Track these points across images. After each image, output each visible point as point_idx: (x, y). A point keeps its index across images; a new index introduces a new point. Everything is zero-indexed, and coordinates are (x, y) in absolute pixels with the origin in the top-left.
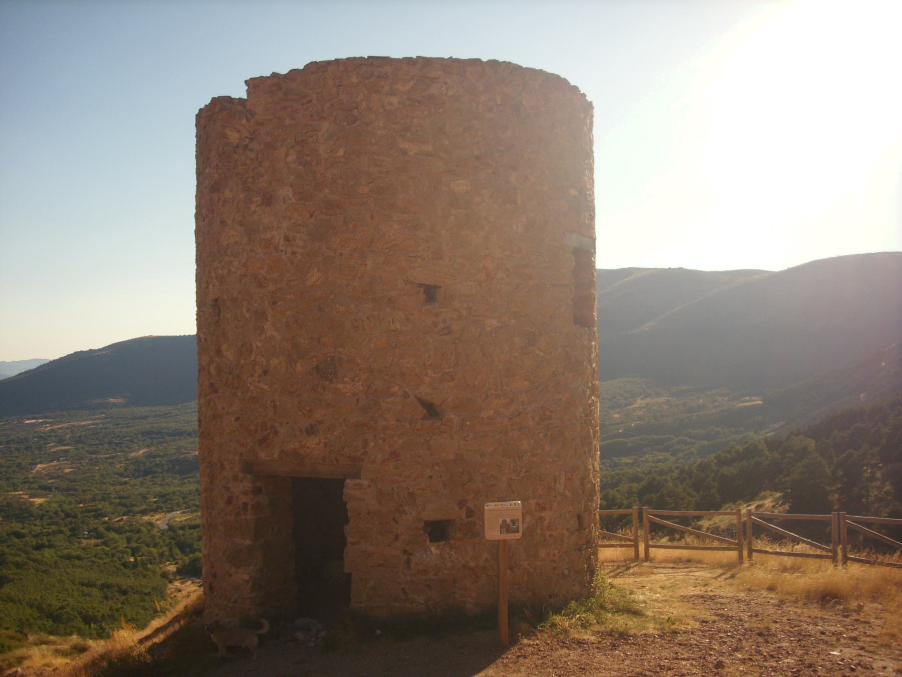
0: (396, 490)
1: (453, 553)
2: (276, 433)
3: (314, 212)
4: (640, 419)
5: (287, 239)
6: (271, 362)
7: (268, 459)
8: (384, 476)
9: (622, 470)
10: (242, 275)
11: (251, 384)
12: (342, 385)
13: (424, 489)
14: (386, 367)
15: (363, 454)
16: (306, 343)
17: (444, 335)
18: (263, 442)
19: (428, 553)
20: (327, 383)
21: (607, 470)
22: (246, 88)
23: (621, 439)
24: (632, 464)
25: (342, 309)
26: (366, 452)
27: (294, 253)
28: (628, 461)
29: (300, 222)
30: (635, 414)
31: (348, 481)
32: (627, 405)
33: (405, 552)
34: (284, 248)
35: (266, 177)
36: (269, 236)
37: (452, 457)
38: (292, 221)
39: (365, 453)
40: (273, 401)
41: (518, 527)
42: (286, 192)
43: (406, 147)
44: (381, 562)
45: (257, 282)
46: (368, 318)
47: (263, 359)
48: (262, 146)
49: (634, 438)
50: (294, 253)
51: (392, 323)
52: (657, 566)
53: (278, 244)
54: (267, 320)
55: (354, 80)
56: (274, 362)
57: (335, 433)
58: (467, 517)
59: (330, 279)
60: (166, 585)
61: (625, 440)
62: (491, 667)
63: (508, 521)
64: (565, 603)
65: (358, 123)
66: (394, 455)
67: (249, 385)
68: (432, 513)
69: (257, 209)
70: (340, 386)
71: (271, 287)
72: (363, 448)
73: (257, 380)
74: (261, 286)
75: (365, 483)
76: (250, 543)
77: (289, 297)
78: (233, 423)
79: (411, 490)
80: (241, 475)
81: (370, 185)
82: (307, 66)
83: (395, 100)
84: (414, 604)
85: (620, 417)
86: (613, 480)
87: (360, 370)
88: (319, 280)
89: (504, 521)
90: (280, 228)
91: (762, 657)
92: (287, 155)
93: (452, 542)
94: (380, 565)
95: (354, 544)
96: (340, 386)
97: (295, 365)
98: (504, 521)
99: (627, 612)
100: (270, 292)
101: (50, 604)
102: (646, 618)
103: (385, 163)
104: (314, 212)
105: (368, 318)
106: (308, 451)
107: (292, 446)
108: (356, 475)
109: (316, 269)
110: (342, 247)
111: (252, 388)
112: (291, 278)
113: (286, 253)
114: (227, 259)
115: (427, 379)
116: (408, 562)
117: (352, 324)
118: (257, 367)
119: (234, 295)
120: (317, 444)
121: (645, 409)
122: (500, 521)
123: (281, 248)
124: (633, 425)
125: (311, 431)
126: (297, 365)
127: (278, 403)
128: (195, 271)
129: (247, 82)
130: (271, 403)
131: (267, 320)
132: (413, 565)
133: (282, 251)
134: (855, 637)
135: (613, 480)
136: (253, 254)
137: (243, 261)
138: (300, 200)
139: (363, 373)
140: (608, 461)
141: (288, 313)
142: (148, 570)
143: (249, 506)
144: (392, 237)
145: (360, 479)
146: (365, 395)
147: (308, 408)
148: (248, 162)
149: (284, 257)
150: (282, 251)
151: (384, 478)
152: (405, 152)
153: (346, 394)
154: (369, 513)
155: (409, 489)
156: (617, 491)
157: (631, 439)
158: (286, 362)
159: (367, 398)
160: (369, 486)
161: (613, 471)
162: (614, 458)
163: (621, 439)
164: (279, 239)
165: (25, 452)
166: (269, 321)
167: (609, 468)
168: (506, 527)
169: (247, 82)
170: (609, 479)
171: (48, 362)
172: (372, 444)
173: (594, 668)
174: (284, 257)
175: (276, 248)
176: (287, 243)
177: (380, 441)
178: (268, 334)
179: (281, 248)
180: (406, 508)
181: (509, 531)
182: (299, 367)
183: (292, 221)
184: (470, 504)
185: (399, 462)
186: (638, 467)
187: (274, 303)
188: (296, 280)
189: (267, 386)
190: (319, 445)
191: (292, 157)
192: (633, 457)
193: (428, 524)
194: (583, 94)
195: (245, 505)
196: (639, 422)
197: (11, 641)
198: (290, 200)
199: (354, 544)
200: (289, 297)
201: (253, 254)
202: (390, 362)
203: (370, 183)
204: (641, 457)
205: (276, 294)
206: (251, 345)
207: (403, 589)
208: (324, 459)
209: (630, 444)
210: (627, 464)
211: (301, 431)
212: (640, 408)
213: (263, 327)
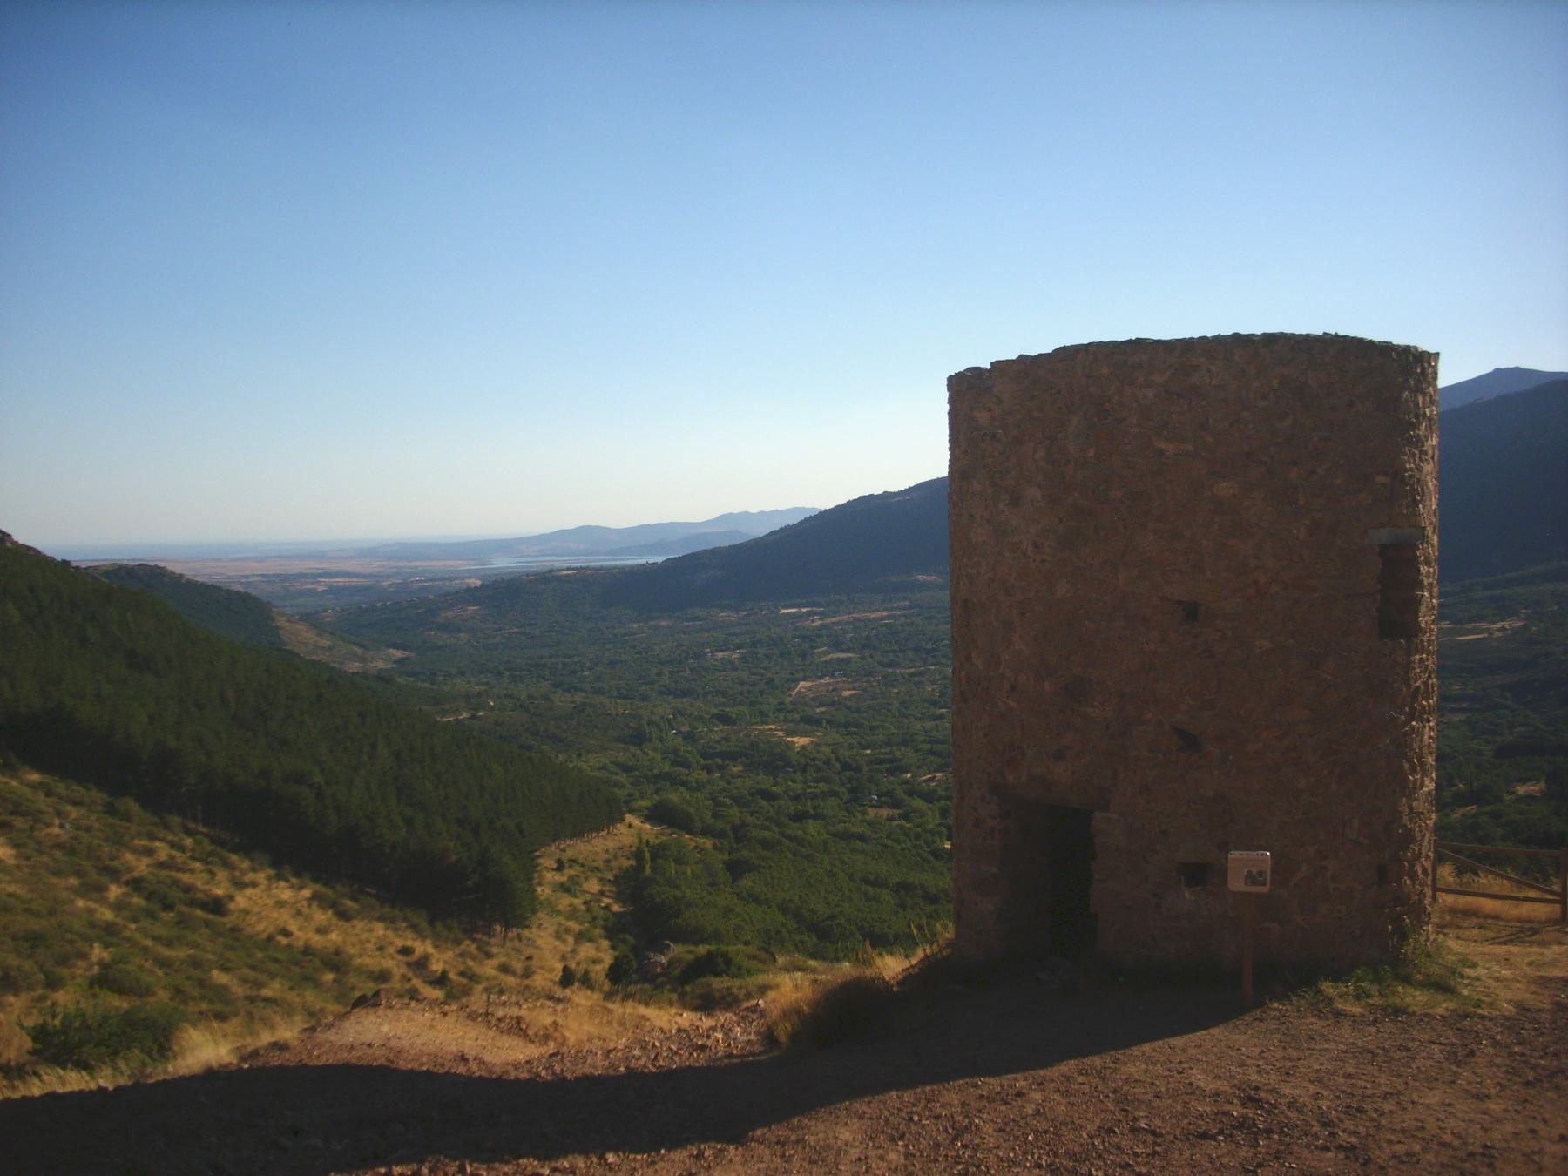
31: (1097, 813)
41: (1265, 879)
63: (1254, 871)
83: (1150, 393)
89: (1250, 872)
98: (1250, 872)
122: (1245, 872)
168: (1251, 879)
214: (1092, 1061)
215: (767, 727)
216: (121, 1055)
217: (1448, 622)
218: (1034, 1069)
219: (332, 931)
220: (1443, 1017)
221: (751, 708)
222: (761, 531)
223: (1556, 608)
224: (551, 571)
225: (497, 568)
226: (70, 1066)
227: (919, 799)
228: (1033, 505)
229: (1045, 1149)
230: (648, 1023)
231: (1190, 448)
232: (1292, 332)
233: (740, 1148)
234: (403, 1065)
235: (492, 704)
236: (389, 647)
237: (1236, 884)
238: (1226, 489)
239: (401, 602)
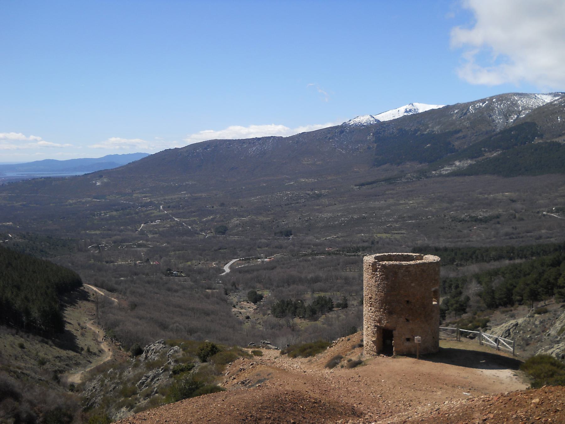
37: (133, 376)
52: (297, 204)
60: (230, 309)
62: (28, 337)
64: (113, 291)
68: (407, 337)
83: (402, 271)
91: (154, 285)
99: (321, 348)
101: (162, 388)
102: (170, 257)
108: (395, 330)
116: (403, 344)
128: (420, 104)
134: (255, 355)
142: (113, 383)
165: (171, 327)
168: (419, 341)
171: (148, 156)
173: (267, 376)
193: (407, 338)
194: (409, 110)
197: (544, 137)
214: (62, 351)
215: (93, 232)
216: (471, 318)
217: (153, 215)
218: (451, 172)
219: (439, 271)
220: (45, 404)
221: (463, 335)
222: (125, 162)
223: (169, 339)
224: (34, 179)
225: (6, 177)
226: (562, 144)
227: (401, 115)
228: (367, 422)
229: (259, 414)
230: (339, 361)
231: (408, 279)
232: (467, 102)
233: (336, 397)
234: (40, 338)
235: (11, 236)
236: (206, 289)
237: (416, 341)
238: (413, 285)
239: (161, 384)
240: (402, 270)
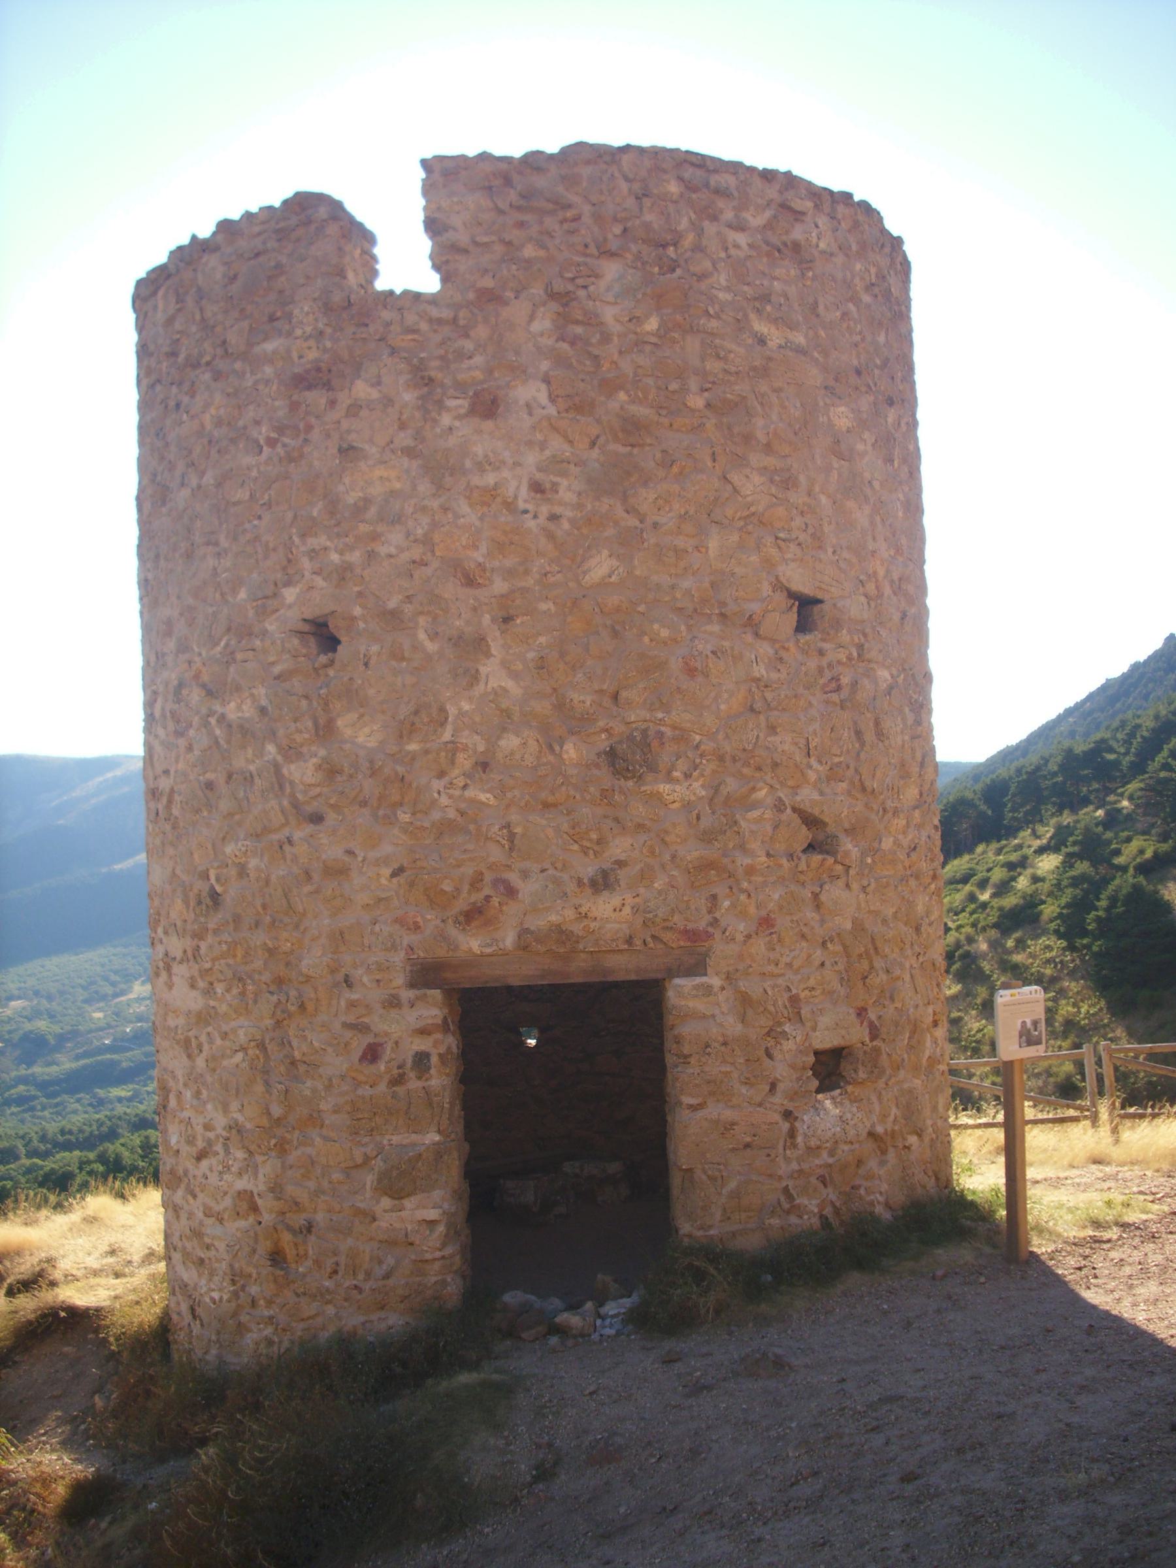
0: (770, 993)
1: (855, 1109)
2: (511, 892)
3: (598, 437)
4: (140, 1018)
5: (537, 488)
6: (502, 743)
7: (488, 950)
8: (751, 966)
9: (113, 1110)
10: (414, 562)
11: (439, 793)
12: (668, 786)
13: (813, 988)
14: (744, 750)
15: (711, 924)
16: (588, 703)
17: (831, 692)
18: (473, 916)
19: (822, 1113)
20: (630, 783)
21: (86, 1112)
22: (423, 175)
23: (108, 1056)
24: (130, 1099)
25: (665, 633)
26: (716, 920)
27: (554, 518)
28: (123, 1094)
29: (567, 454)
30: (131, 1011)
32: (116, 995)
33: (788, 1115)
34: (530, 507)
35: (478, 360)
36: (490, 479)
38: (547, 453)
39: (715, 922)
40: (508, 826)
42: (532, 392)
43: (765, 330)
44: (748, 1139)
45: (459, 575)
46: (713, 652)
47: (477, 738)
48: (471, 296)
49: (131, 1053)
50: (554, 518)
51: (755, 664)
53: (516, 497)
54: (488, 655)
55: (674, 188)
56: (510, 742)
57: (656, 885)
58: (871, 1041)
59: (638, 573)
61: (115, 1057)
63: (1029, 1025)
65: (679, 272)
66: (766, 922)
67: (436, 795)
69: (457, 423)
70: (664, 788)
71: (500, 586)
72: (709, 912)
73: (462, 784)
74: (470, 582)
75: (716, 982)
76: (437, 1138)
77: (543, 606)
78: (384, 881)
79: (794, 991)
80: (407, 994)
81: (706, 394)
82: (565, 151)
83: (742, 239)
84: (806, 1217)
85: (105, 1016)
86: (102, 1129)
87: (702, 756)
88: (613, 572)
90: (520, 465)
92: (532, 318)
93: (850, 1088)
94: (747, 1146)
95: (694, 1108)
96: (664, 788)
97: (561, 748)
100: (495, 597)
103: (732, 355)
104: (598, 437)
105: (713, 652)
106: (593, 925)
107: (554, 918)
108: (698, 967)
109: (605, 553)
110: (659, 509)
111: (444, 800)
112: (548, 569)
113: (535, 517)
114: (363, 528)
115: (812, 776)
117: (686, 663)
118: (461, 756)
119: (392, 604)
120: (615, 910)
121: (148, 1002)
123: (521, 505)
124: (128, 1030)
125: (602, 883)
126: (565, 748)
127: (518, 830)
129: (425, 163)
130: (500, 829)
131: (488, 655)
132: (799, 1139)
133: (526, 512)
135: (102, 1129)
136: (450, 516)
137: (420, 531)
138: (567, 411)
139: (707, 761)
140: (88, 1097)
141: (542, 640)
143: (434, 1059)
144: (749, 499)
145: (705, 975)
146: (710, 805)
147: (594, 836)
148: (424, 326)
149: (531, 524)
150: (526, 512)
151: (751, 970)
152: (762, 341)
153: (671, 806)
154: (725, 1044)
155: (790, 990)
156: (123, 1145)
157: (128, 1054)
158: (538, 741)
159: (713, 813)
160: (723, 988)
161: (96, 1113)
162: (98, 1090)
163: (108, 1056)
164: (518, 488)
166: (492, 655)
167: (90, 1109)
169: (425, 163)
170: (95, 1127)
172: (727, 903)
174: (531, 524)
175: (510, 506)
176: (539, 496)
177: (743, 897)
178: (493, 683)
179: (521, 505)
180: (787, 1028)
181: (1030, 1043)
182: (571, 751)
183: (547, 453)
184: (872, 1016)
185: (774, 936)
186: (141, 1103)
187: (507, 620)
188: (559, 572)
189: (488, 795)
190: (620, 910)
191: (544, 323)
192: (131, 1086)
195: (421, 1060)
196: (139, 1024)
198: (543, 408)
199: (694, 1108)
200: (543, 606)
201: (450, 516)
202: (754, 741)
203: (706, 390)
204: (145, 1085)
205: (513, 601)
206: (442, 710)
207: (786, 1190)
208: (629, 941)
209: (124, 1065)
210: (120, 1100)
211: (580, 882)
212: (139, 1000)
213: (477, 670)
231: (800, 339)
240: (741, 228)
